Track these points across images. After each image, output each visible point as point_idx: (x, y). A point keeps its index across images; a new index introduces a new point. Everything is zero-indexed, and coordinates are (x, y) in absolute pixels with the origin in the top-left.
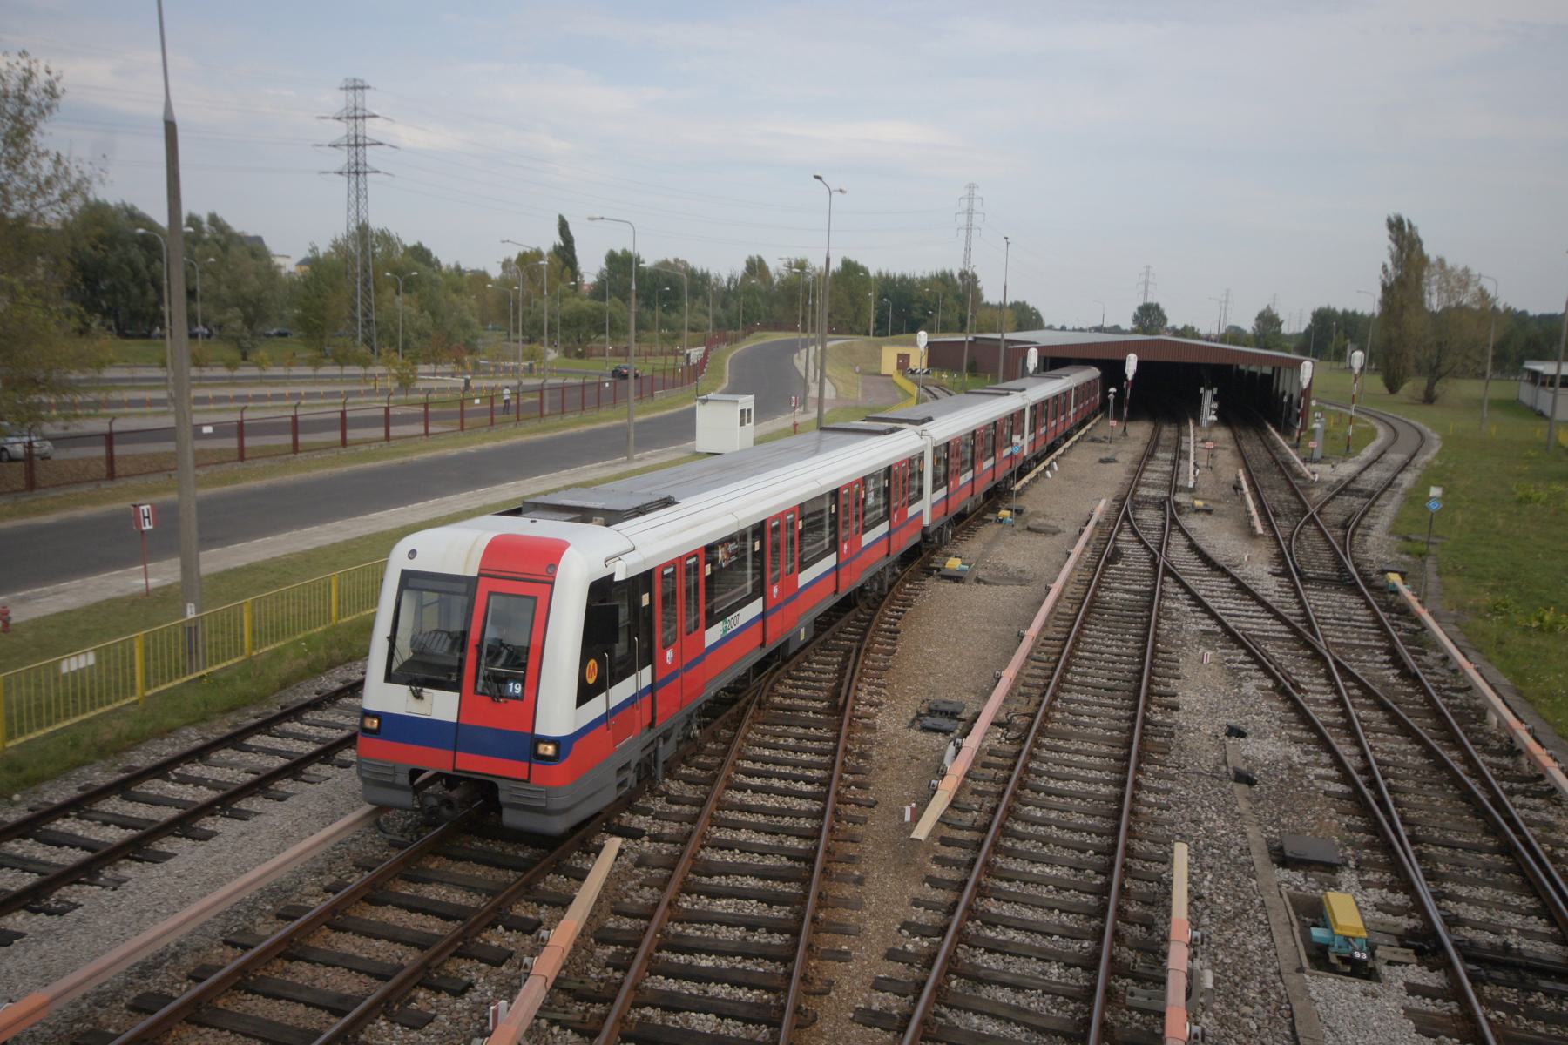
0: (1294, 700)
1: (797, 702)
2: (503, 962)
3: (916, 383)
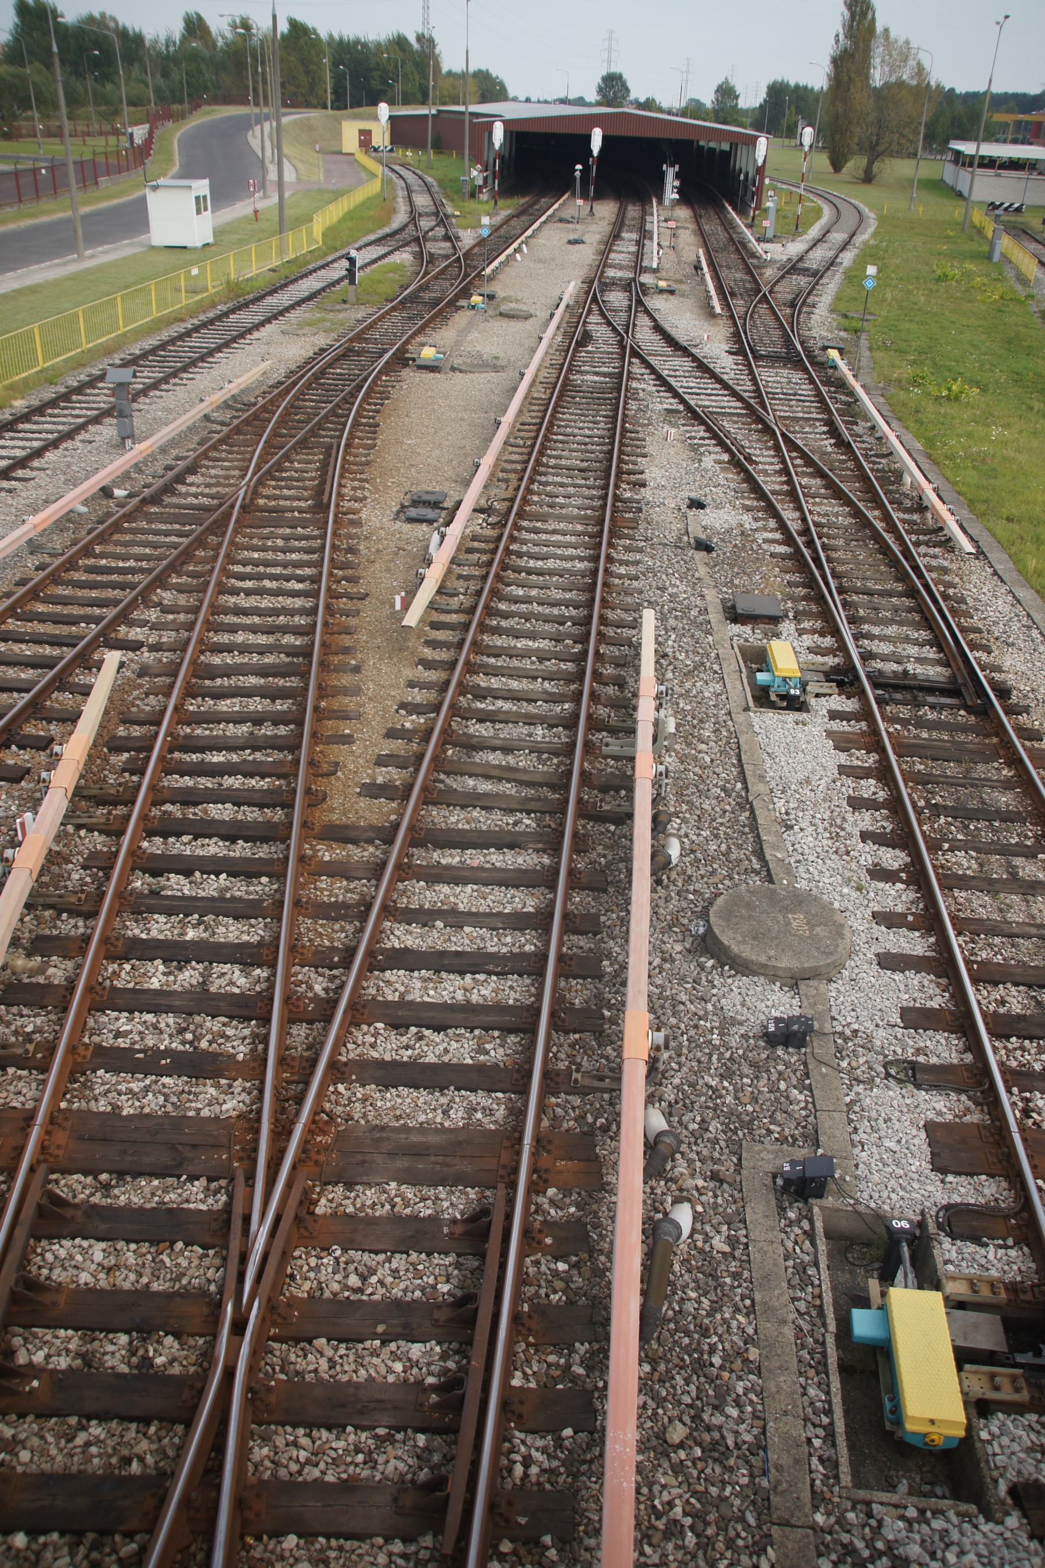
0: (746, 471)
1: (282, 503)
2: (22, 778)
3: (380, 161)
